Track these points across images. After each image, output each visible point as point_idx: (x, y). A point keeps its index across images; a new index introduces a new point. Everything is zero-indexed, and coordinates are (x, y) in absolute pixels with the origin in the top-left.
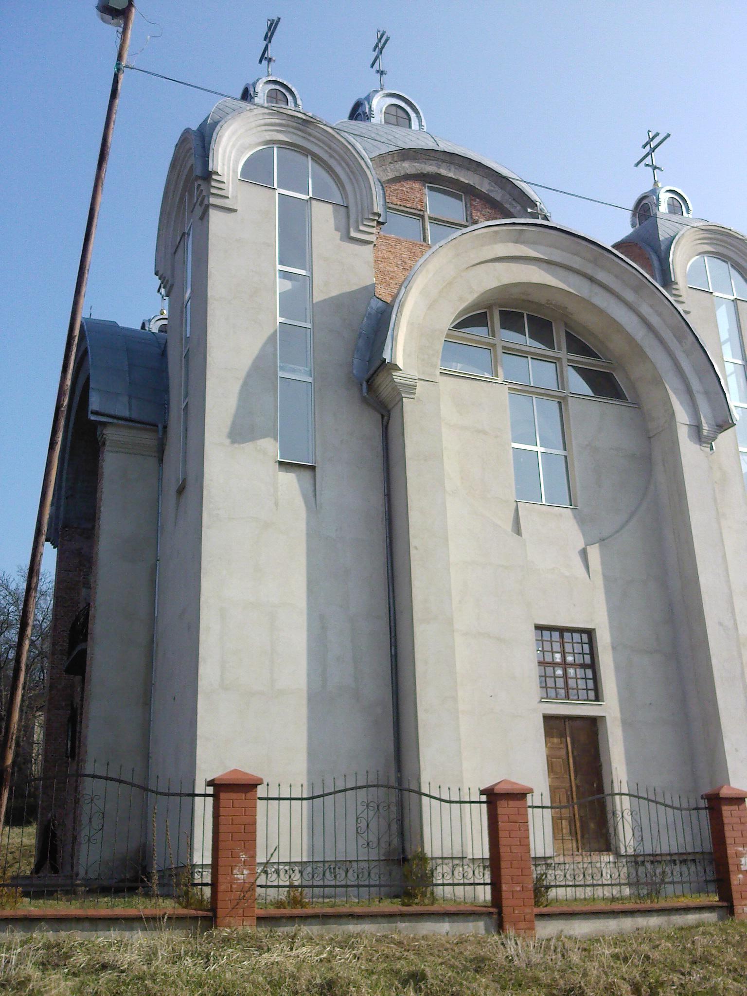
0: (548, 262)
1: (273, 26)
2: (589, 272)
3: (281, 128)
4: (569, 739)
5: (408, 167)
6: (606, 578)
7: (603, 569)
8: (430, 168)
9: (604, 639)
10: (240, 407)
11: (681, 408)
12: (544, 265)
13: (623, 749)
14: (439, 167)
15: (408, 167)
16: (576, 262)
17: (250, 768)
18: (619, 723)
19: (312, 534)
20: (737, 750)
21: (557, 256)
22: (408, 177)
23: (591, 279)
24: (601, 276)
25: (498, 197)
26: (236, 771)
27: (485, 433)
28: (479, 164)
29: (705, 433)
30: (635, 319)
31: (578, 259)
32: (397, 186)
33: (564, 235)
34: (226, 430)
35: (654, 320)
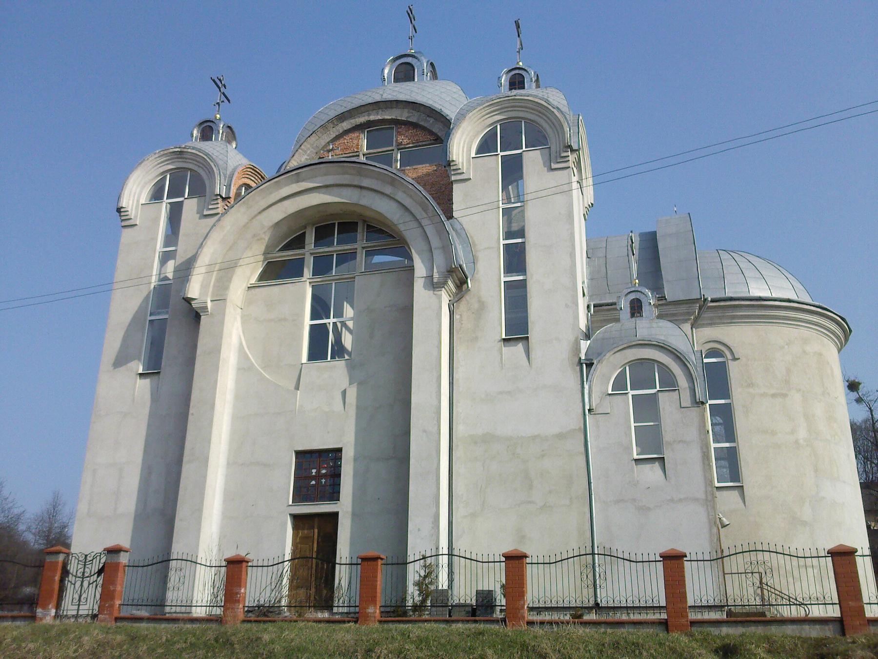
0: (327, 186)
1: (410, 13)
2: (356, 183)
3: (170, 161)
4: (316, 531)
5: (346, 125)
6: (358, 408)
7: (357, 402)
8: (362, 119)
9: (348, 456)
10: (122, 346)
11: (422, 265)
12: (324, 190)
13: (349, 534)
14: (369, 115)
15: (346, 125)
16: (346, 179)
17: (681, 548)
18: (349, 516)
19: (152, 415)
20: (419, 530)
21: (330, 180)
22: (347, 132)
23: (361, 188)
24: (366, 183)
25: (413, 119)
26: (673, 549)
27: (285, 320)
28: (397, 101)
29: (435, 280)
30: (394, 205)
31: (346, 176)
32: (342, 141)
33: (331, 165)
34: (112, 361)
35: (407, 202)
